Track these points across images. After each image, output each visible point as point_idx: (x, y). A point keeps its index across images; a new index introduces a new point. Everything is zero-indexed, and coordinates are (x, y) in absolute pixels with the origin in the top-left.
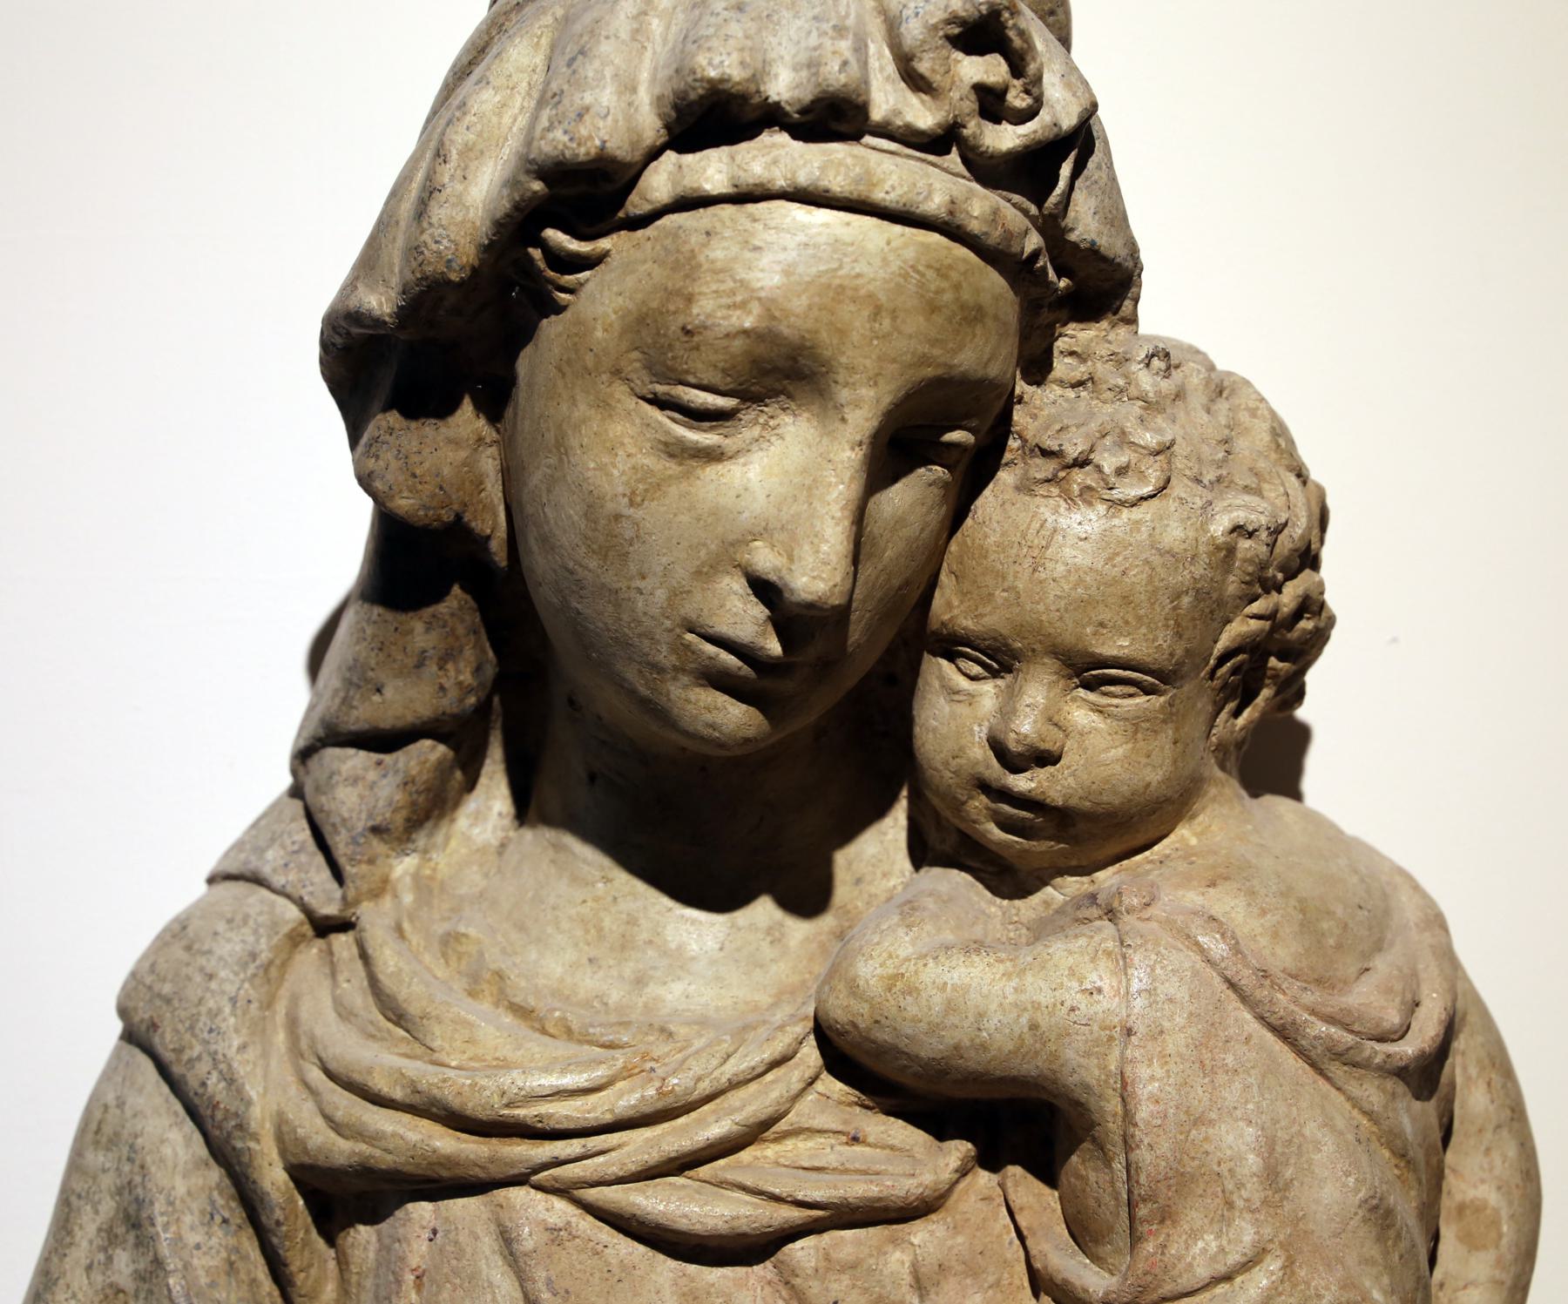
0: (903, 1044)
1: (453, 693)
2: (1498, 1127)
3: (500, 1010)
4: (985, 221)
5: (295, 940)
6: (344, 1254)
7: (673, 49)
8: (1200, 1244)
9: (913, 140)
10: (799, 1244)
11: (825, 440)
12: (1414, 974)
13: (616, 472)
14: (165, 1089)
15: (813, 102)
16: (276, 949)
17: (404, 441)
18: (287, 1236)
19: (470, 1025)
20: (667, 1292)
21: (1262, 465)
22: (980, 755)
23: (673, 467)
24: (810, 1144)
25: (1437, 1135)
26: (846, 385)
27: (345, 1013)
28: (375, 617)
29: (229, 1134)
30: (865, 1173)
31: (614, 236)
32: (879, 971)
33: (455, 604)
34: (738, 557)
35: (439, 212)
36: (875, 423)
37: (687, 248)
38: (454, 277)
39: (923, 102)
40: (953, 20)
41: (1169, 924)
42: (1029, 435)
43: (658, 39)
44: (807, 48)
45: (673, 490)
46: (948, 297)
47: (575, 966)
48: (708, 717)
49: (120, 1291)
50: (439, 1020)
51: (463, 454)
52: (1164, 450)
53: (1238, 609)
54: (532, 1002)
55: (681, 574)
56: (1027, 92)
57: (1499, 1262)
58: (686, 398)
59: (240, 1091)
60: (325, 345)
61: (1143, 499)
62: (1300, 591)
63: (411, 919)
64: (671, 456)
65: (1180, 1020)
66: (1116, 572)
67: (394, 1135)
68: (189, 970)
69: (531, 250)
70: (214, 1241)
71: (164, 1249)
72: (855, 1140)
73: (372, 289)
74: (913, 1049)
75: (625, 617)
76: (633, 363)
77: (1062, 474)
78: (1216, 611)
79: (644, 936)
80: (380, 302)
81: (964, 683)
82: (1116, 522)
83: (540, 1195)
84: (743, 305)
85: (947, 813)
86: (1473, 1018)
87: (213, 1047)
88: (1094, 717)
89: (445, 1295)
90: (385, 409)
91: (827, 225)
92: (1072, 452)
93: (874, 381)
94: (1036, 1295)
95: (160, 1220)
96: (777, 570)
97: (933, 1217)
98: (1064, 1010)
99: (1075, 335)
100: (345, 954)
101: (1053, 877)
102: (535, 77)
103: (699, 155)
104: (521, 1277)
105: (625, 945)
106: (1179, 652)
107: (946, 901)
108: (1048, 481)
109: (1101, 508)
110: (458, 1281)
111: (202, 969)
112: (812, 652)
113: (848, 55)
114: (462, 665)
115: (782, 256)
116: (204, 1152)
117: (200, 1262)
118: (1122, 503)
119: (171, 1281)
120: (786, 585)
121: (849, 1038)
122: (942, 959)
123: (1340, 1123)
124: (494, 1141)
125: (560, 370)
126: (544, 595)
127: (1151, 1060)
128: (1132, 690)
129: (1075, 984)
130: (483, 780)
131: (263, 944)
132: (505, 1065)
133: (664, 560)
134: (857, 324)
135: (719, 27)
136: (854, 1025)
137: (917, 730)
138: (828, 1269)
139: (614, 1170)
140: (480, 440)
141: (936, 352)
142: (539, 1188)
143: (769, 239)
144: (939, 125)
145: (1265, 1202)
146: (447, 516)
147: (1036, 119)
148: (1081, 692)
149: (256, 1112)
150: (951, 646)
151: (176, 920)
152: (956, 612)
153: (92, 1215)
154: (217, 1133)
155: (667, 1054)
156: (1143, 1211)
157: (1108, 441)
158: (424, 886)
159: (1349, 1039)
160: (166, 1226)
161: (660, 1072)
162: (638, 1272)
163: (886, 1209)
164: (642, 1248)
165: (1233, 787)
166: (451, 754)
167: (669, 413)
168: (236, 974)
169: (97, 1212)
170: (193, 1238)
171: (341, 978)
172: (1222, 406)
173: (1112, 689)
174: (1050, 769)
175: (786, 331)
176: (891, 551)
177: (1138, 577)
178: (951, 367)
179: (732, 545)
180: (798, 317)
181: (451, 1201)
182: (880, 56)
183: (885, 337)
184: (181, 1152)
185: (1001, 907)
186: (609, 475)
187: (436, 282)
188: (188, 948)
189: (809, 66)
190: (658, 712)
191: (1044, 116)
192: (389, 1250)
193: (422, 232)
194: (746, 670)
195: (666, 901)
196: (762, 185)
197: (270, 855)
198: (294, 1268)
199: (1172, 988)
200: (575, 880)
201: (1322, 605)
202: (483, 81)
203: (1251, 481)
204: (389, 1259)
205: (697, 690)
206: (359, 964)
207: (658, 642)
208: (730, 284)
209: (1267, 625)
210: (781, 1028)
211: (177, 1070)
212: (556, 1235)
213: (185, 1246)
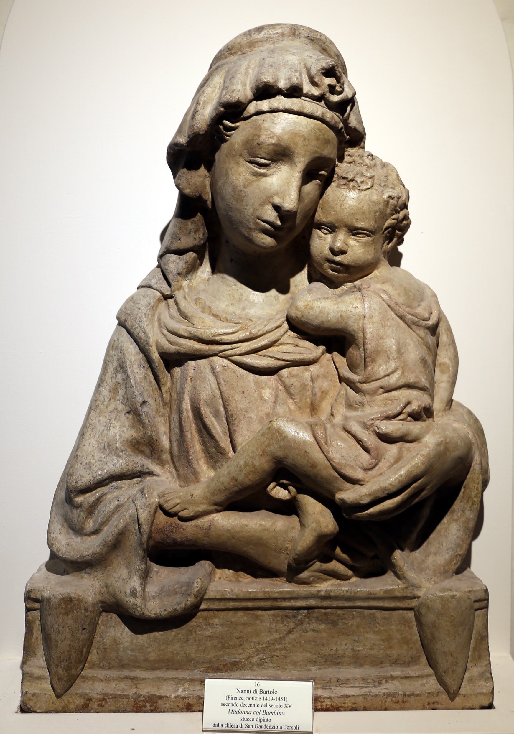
0: (309, 321)
1: (198, 240)
2: (449, 345)
3: (210, 315)
4: (330, 118)
5: (159, 301)
6: (173, 375)
7: (255, 76)
8: (382, 367)
9: (314, 98)
10: (283, 370)
11: (292, 171)
12: (431, 306)
13: (240, 180)
14: (129, 336)
15: (290, 88)
16: (155, 302)
17: (187, 176)
18: (159, 370)
19: (203, 319)
20: (251, 382)
21: (395, 182)
22: (327, 252)
23: (254, 178)
24: (286, 347)
25: (436, 345)
26: (297, 157)
27: (172, 317)
28: (179, 221)
29: (145, 345)
30: (299, 353)
31: (240, 122)
32: (303, 304)
33: (198, 218)
34: (270, 200)
35: (198, 117)
36: (304, 167)
37: (259, 124)
38: (201, 133)
39: (316, 89)
40: (323, 68)
41: (374, 292)
42: (339, 174)
43: (251, 74)
44: (288, 75)
45: (255, 184)
46: (321, 137)
47: (227, 305)
48: (262, 241)
49: (119, 383)
50: (195, 317)
51: (202, 179)
52: (372, 177)
53: (389, 217)
54: (218, 313)
55: (256, 205)
56: (341, 87)
57: (449, 377)
58: (258, 161)
59: (147, 335)
60: (168, 153)
61: (367, 189)
62: (404, 214)
63: (188, 295)
64: (254, 175)
65: (377, 314)
66: (361, 207)
67: (185, 344)
68: (134, 308)
69: (220, 126)
70: (141, 372)
71: (129, 373)
72: (297, 346)
73: (180, 137)
74: (311, 323)
75: (242, 216)
76: (245, 153)
77: (347, 183)
78: (384, 217)
79: (245, 298)
80: (182, 140)
81: (323, 235)
82: (361, 194)
83: (221, 359)
84: (272, 138)
85: (319, 269)
86: (443, 319)
87: (140, 325)
88: (355, 242)
89: (198, 382)
90: (183, 168)
91: (292, 118)
92: (350, 177)
93: (304, 156)
94: (340, 383)
95: (128, 366)
96: (280, 203)
97: (316, 364)
98: (349, 312)
99: (350, 151)
100: (172, 304)
101: (344, 283)
102: (221, 85)
103: (261, 102)
104: (216, 378)
105: (240, 300)
106: (376, 226)
107: (318, 289)
108: (344, 185)
109: (357, 191)
110: (201, 379)
111: (137, 307)
112: (288, 225)
113: (298, 76)
114: (200, 233)
115: (281, 126)
116: (139, 350)
117: (138, 376)
118: (362, 190)
119: (131, 381)
120: (282, 206)
121: (296, 320)
122: (319, 301)
123: (415, 339)
124: (210, 345)
125: (226, 156)
126: (221, 213)
127: (370, 324)
128: (364, 236)
129: (351, 306)
130: (204, 263)
131: (152, 301)
132: (212, 327)
133: (252, 201)
134: (300, 142)
135: (266, 70)
136: (297, 317)
137: (311, 247)
138: (290, 376)
139: (239, 352)
140: (206, 176)
141: (319, 150)
142: (220, 357)
143: (278, 121)
144: (320, 94)
145: (397, 357)
146: (197, 195)
147: (343, 94)
148: (352, 237)
149: (151, 340)
150: (320, 226)
151: (130, 297)
152: (321, 217)
153: (112, 366)
154: (142, 345)
155: (251, 325)
156: (368, 360)
157: (358, 175)
158: (190, 288)
159: (417, 319)
160: (130, 368)
161: (250, 329)
162: (244, 377)
163: (305, 362)
164: (245, 371)
165: (387, 263)
166: (197, 256)
167: (254, 165)
168: (146, 308)
169: (113, 365)
170: (136, 371)
171: (171, 309)
172: (385, 169)
173: (360, 235)
174: (344, 255)
175: (283, 144)
176: (307, 201)
177: (366, 207)
178: (322, 154)
179: (269, 197)
180: (286, 140)
181: (199, 361)
182: (305, 78)
183: (306, 146)
184: (133, 350)
185: (331, 291)
186: (239, 180)
187: (197, 134)
188: (134, 303)
189: (288, 79)
190: (250, 240)
191: (344, 94)
192: (184, 373)
193: (193, 122)
194: (272, 229)
195: (250, 290)
196: (277, 108)
197: (153, 281)
198: (161, 378)
199: (375, 306)
200: (228, 285)
201: (409, 218)
202: (209, 86)
203: (392, 186)
204: (184, 375)
205: (260, 234)
206: (175, 306)
207: (250, 222)
208: (269, 132)
209: (396, 221)
210: (279, 319)
211: (132, 331)
212: (225, 368)
213: (134, 373)
